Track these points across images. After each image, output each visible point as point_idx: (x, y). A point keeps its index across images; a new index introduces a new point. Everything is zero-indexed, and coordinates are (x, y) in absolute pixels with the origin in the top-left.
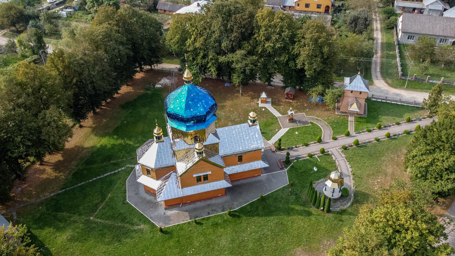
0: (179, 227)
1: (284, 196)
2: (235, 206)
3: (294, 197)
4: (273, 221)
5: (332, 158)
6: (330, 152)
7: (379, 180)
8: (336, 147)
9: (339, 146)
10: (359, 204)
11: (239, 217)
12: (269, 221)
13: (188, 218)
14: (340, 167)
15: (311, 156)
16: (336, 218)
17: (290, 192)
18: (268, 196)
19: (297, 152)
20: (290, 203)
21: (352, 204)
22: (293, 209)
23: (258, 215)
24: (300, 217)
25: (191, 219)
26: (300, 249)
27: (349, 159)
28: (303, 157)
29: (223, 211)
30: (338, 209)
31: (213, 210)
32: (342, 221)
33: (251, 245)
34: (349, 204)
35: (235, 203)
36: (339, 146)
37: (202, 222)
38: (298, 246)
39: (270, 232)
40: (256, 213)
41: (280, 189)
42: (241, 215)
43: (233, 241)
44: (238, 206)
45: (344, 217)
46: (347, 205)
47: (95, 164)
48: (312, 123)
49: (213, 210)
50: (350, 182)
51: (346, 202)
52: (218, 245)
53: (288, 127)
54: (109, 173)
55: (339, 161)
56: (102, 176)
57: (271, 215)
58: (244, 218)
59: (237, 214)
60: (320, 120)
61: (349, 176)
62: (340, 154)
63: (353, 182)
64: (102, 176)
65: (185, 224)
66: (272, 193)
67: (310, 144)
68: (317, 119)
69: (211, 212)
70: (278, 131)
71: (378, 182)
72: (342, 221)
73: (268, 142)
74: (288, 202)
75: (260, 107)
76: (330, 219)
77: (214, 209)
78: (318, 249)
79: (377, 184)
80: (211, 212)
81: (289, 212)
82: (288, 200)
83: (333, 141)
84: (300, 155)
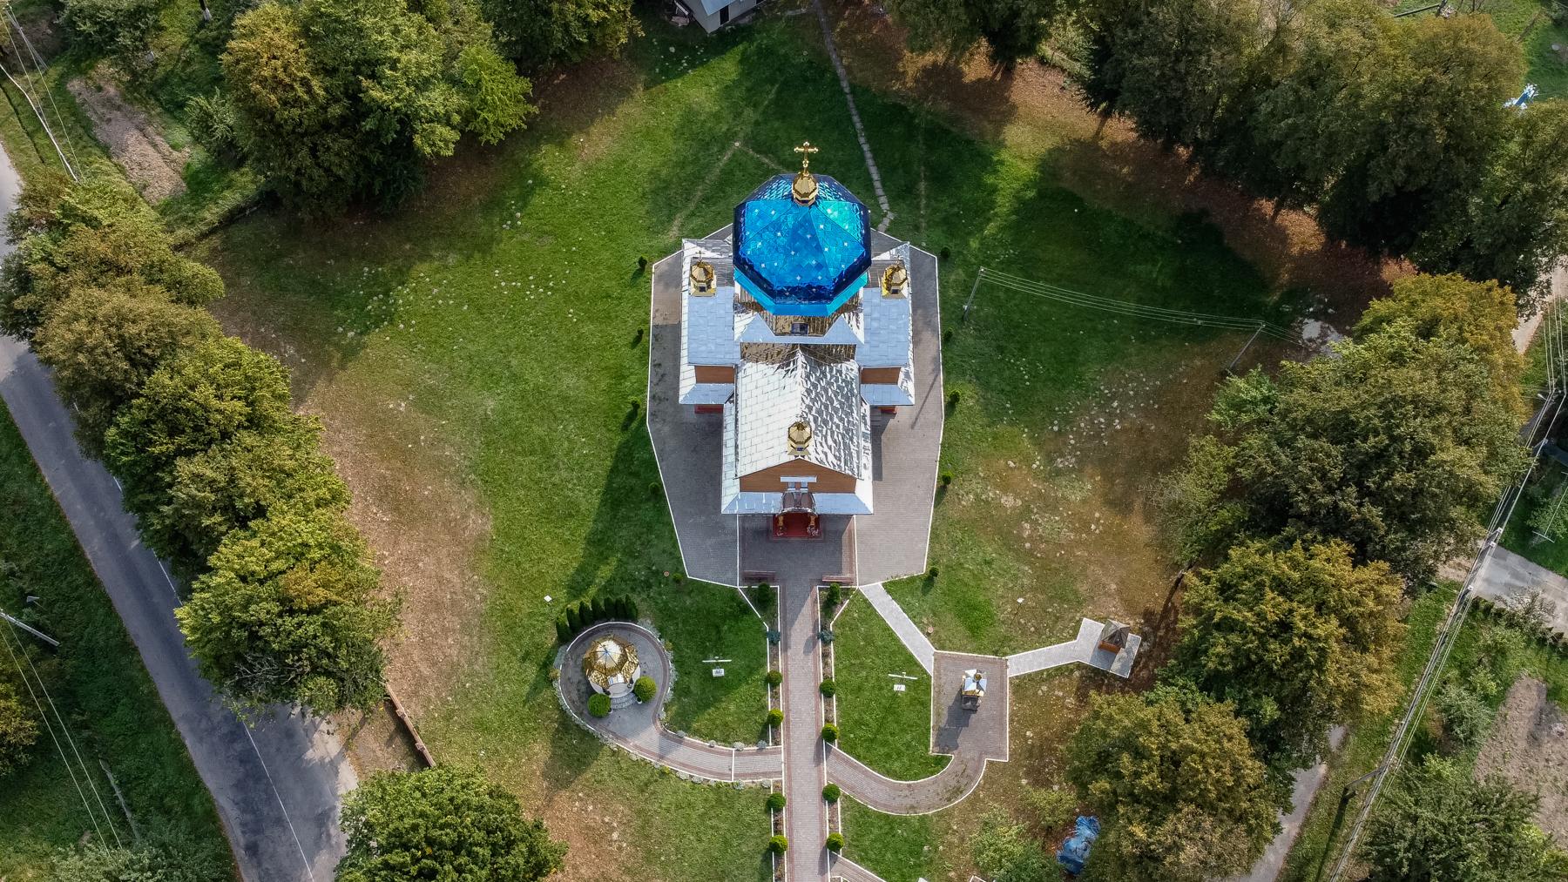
0: (643, 300)
1: (652, 551)
2: (659, 426)
3: (642, 575)
4: (589, 500)
5: (747, 742)
6: (770, 746)
7: (615, 836)
8: (789, 777)
9: (790, 788)
10: (557, 730)
11: (625, 427)
12: (590, 492)
13: (660, 321)
14: (702, 748)
15: (773, 681)
16: (538, 646)
17: (657, 573)
18: (662, 510)
19: (801, 648)
20: (625, 559)
21: (563, 712)
22: (603, 559)
23: (614, 471)
24: (575, 565)
25: (656, 326)
26: (488, 528)
27: (724, 796)
28: (775, 657)
29: (653, 397)
30: (558, 670)
31: (663, 376)
32: (524, 659)
33: (539, 430)
34: (564, 702)
35: (666, 429)
36: (790, 788)
37: (639, 346)
38: (495, 526)
39: (557, 481)
40: (621, 467)
41: (675, 544)
42: (627, 435)
43: (565, 399)
44: (656, 432)
45: (531, 672)
46: (562, 693)
47: (1299, 414)
48: (940, 762)
49: (663, 376)
50: (636, 747)
51: (575, 696)
52: (567, 370)
53: (937, 669)
54: (875, 176)
55: (728, 758)
56: (870, 162)
57: (603, 502)
58: (619, 439)
59: (634, 425)
60: (949, 800)
61: (661, 757)
62: (756, 775)
63: (636, 755)
64: (870, 162)
65: (648, 314)
66: (670, 524)
67: (828, 704)
68: (958, 791)
69: (661, 371)
70: (928, 635)
71: (613, 829)
72: (524, 659)
73: (879, 584)
74: (631, 553)
75: (1079, 622)
76: (540, 631)
77: (666, 378)
78: (473, 569)
79: (603, 822)
80: (661, 371)
81: (599, 544)
82: (637, 557)
83: (820, 781)
84: (786, 649)
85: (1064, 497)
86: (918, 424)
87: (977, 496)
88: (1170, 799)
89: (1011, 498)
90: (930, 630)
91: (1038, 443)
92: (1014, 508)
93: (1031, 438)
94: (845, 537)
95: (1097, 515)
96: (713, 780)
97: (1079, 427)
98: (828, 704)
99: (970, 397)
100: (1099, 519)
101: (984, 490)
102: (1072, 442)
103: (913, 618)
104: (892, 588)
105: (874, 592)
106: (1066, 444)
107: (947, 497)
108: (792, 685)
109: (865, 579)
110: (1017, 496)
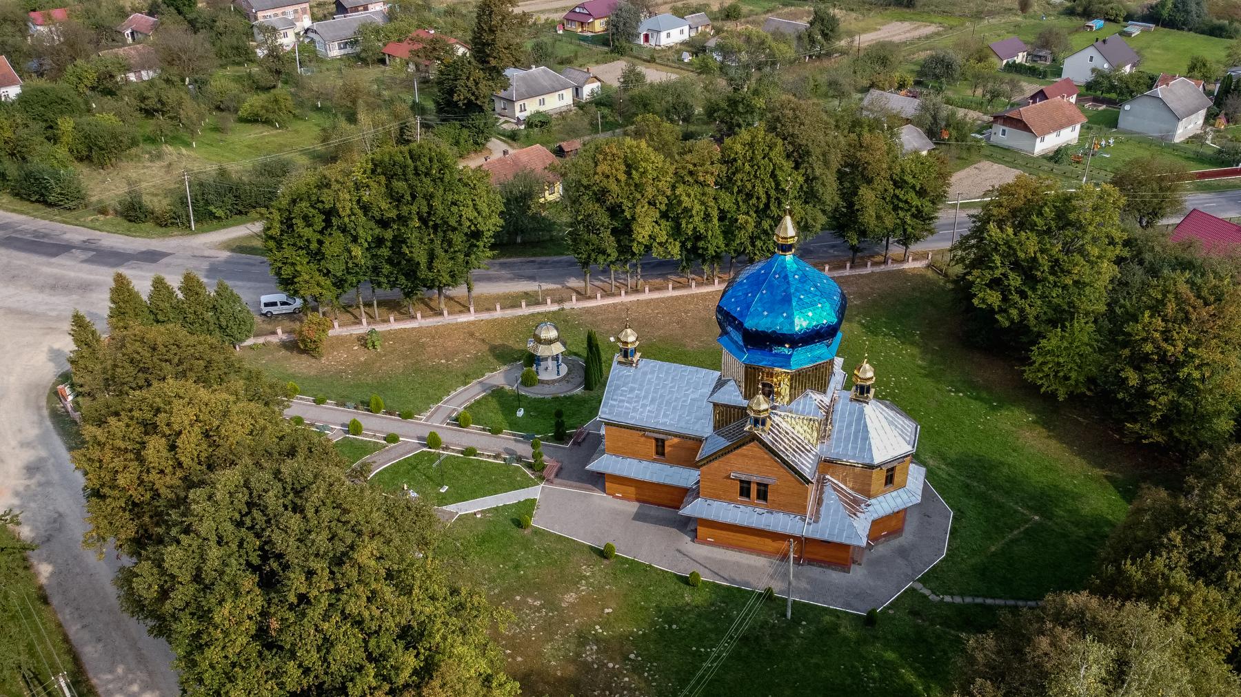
67: (458, 452)
73: (538, 497)
83: (403, 436)
85: (552, 640)
86: (678, 554)
87: (586, 578)
88: (376, 660)
89: (572, 600)
90: (479, 516)
91: (623, 639)
92: (562, 600)
93: (631, 633)
94: (590, 486)
95: (519, 659)
96: (453, 393)
97: (625, 676)
98: (458, 452)
99: (689, 597)
100: (514, 659)
101: (589, 584)
102: (611, 665)
103: (497, 509)
104: (530, 504)
105: (534, 492)
106: (612, 659)
107: (595, 557)
108: (401, 424)
109: (546, 490)
110: (573, 605)
